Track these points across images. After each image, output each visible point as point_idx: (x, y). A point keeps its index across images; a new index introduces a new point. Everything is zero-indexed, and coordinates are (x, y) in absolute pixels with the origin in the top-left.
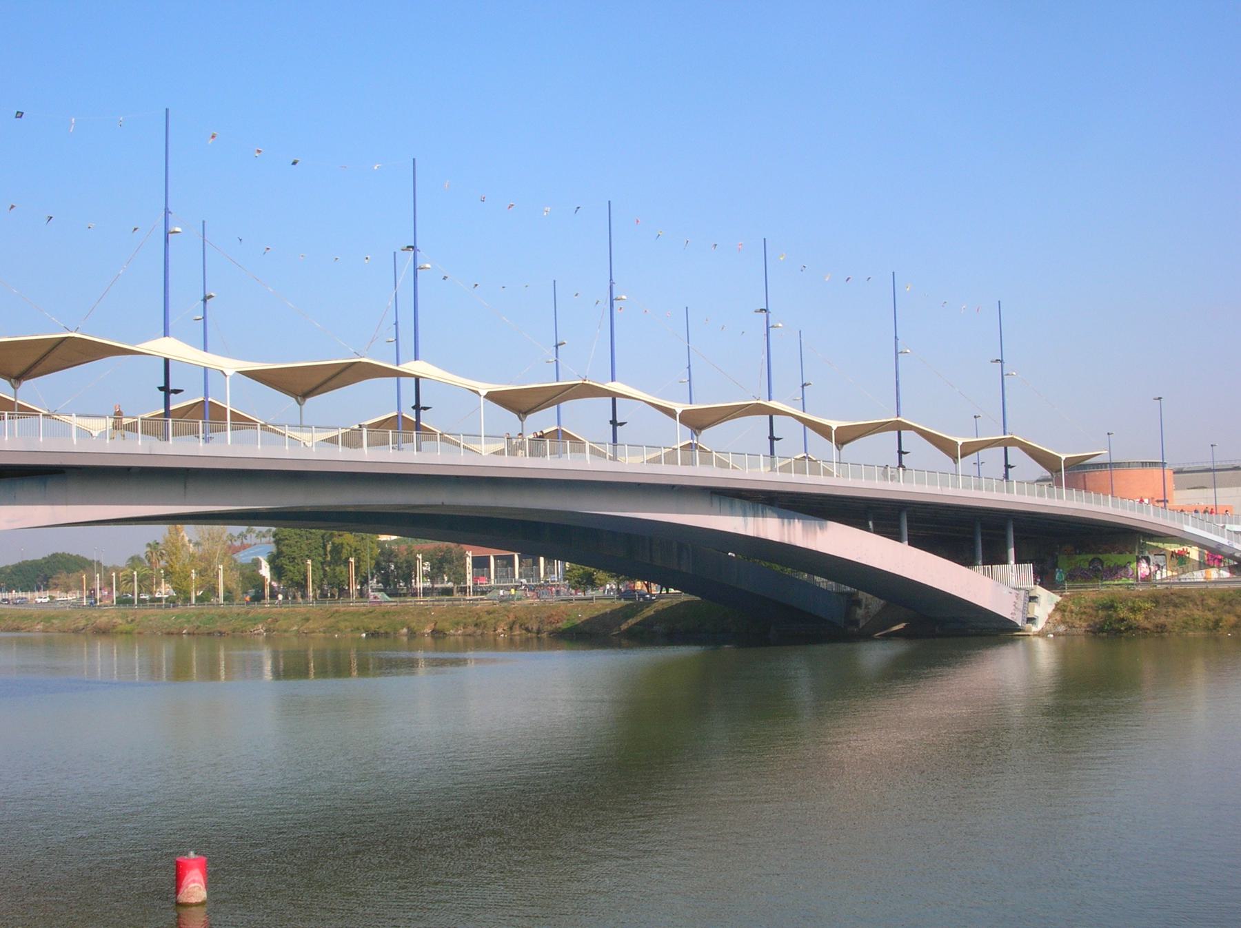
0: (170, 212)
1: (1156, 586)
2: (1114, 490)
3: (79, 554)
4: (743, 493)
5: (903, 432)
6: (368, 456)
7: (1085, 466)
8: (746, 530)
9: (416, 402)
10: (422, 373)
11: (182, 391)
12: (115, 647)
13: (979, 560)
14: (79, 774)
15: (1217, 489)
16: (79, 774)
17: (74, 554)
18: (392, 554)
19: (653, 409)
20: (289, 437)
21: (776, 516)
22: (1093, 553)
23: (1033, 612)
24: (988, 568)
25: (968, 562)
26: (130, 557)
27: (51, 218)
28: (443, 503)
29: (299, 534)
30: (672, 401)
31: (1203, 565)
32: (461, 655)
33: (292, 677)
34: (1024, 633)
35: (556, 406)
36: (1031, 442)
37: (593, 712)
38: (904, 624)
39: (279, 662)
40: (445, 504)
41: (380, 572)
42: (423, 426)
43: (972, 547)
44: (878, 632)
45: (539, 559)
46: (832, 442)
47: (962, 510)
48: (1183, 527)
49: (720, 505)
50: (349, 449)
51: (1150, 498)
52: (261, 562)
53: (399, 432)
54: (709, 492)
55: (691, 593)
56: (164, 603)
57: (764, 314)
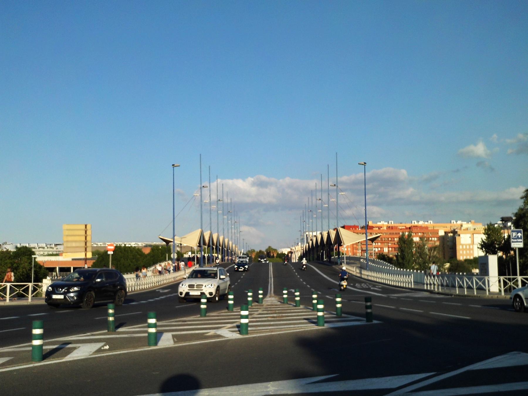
1: (227, 256)
2: (202, 170)
3: (118, 244)
4: (402, 299)
6: (349, 316)
10: (339, 231)
12: (380, 290)
13: (252, 177)
14: (232, 236)
16: (232, 236)
17: (144, 252)
19: (430, 392)
22: (100, 268)
24: (67, 233)
28: (48, 260)
29: (439, 260)
36: (165, 237)
38: (13, 358)
41: (341, 273)
42: (365, 318)
43: (199, 276)
45: (106, 330)
46: (342, 252)
48: (221, 236)
51: (388, 238)
54: (205, 187)
55: (168, 289)
57: (300, 232)
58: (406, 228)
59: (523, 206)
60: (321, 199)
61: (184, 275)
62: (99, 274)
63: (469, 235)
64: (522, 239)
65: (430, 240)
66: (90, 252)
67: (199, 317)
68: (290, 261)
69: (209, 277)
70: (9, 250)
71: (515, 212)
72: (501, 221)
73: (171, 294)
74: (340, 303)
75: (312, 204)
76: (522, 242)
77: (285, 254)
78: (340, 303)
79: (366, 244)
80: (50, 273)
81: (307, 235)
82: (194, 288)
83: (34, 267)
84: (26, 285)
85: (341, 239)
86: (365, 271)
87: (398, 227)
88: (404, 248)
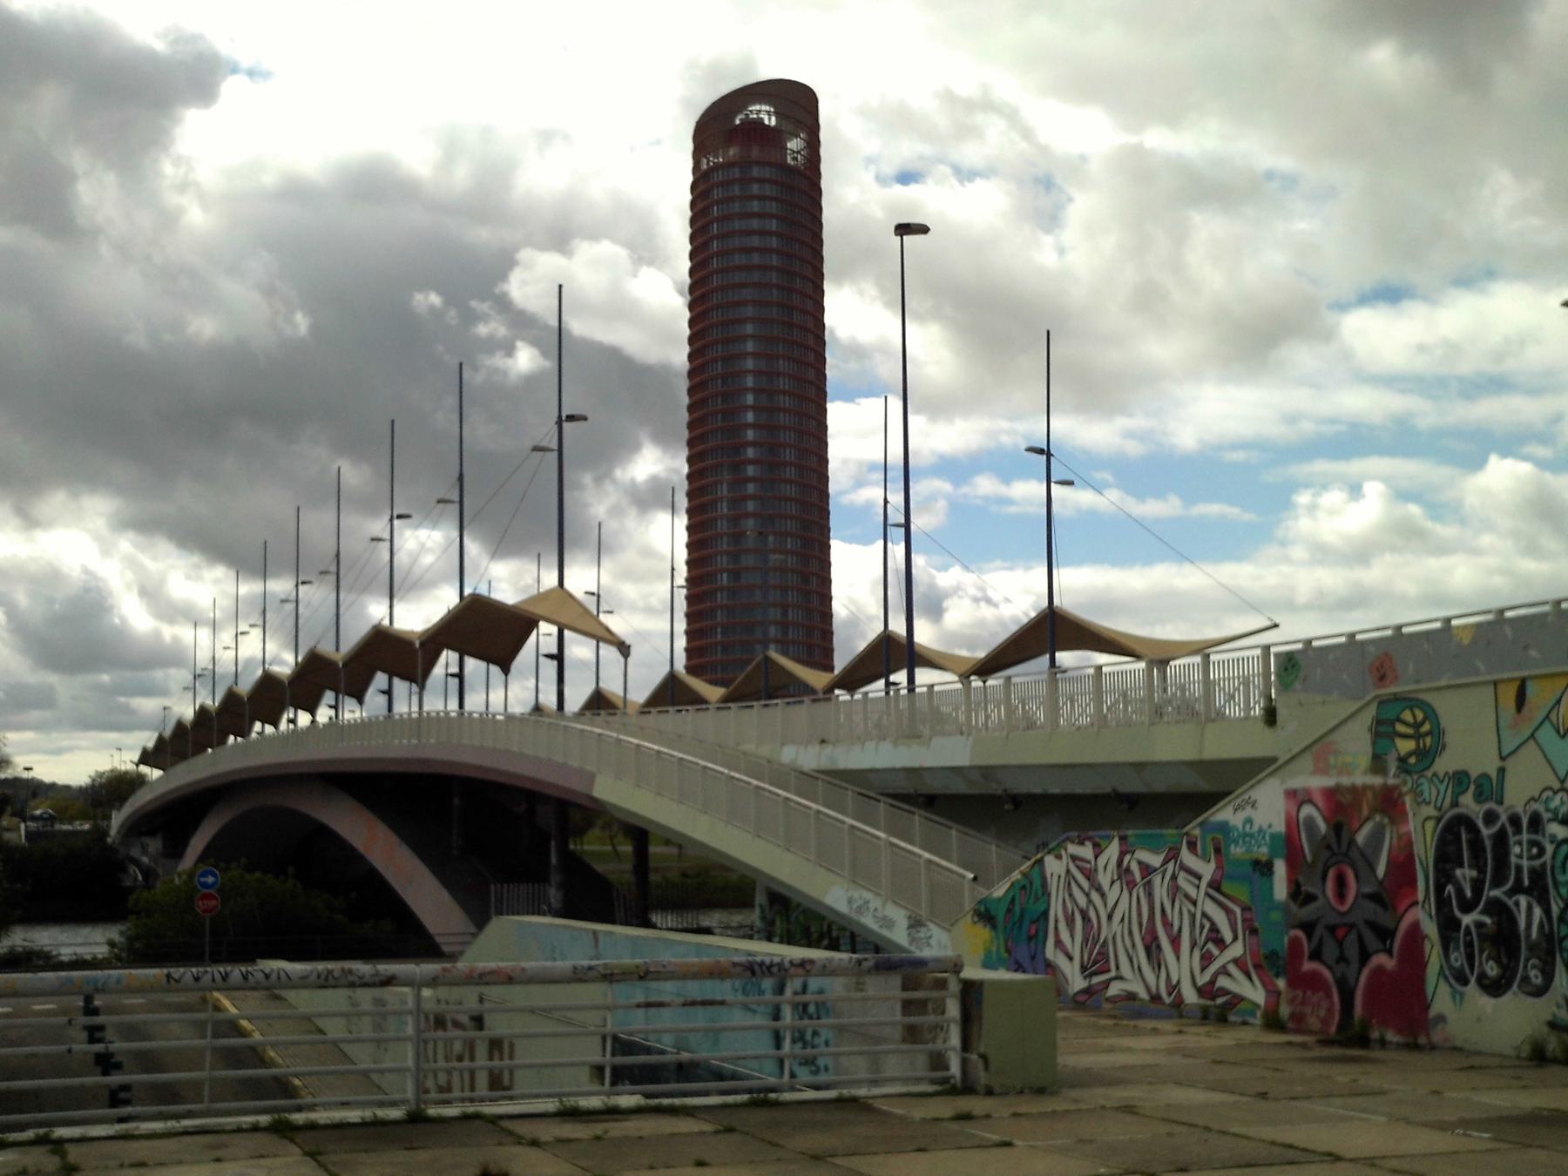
0: (1052, 455)
5: (601, 644)
7: (777, 1104)
8: (605, 612)
9: (1049, 603)
10: (941, 824)
11: (585, 419)
15: (1060, 570)
18: (1329, 847)
20: (1071, 958)
21: (915, 645)
23: (746, 453)
25: (996, 969)
26: (893, 229)
27: (1276, 626)
30: (1255, 776)
31: (175, 849)
32: (802, 699)
33: (580, 968)
34: (188, 1016)
35: (541, 590)
37: (1236, 834)
39: (667, 1097)
40: (232, 574)
44: (548, 855)
47: (626, 744)
49: (409, 572)
50: (906, 926)
52: (122, 825)
53: (865, 999)
56: (719, 637)
73: (1508, 881)
83: (632, 1040)
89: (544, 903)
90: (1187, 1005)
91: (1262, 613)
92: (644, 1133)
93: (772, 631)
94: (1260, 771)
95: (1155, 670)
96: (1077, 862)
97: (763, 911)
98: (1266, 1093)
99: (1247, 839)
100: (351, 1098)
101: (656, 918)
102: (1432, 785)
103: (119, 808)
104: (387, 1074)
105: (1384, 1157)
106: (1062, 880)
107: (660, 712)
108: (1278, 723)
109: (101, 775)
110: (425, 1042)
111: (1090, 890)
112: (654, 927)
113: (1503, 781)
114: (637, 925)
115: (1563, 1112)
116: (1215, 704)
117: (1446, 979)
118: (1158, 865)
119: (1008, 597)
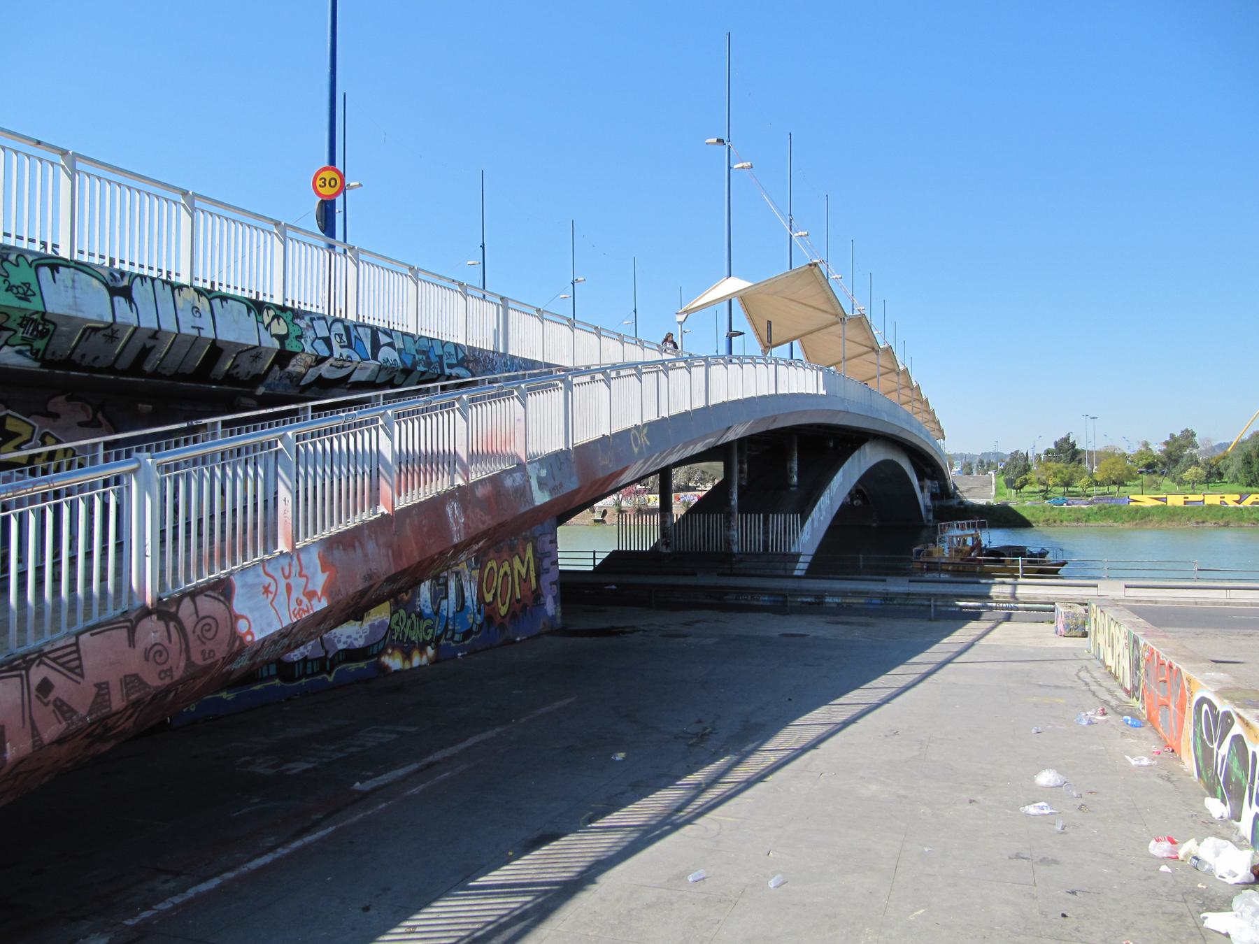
11: (744, 334)
58: (1079, 796)
59: (257, 357)
60: (726, 139)
61: (1201, 483)
62: (1165, 649)
63: (511, 352)
64: (42, 370)
65: (271, 663)
66: (163, 332)
67: (834, 594)
68: (605, 465)
69: (76, 535)
70: (1178, 434)
71: (1249, 871)
72: (355, 552)
74: (1036, 795)
75: (182, 362)
76: (292, 620)
77: (689, 411)
78: (1036, 795)
79: (708, 365)
80: (667, 513)
81: (512, 393)
82: (136, 448)
83: (469, 638)
84: (1215, 741)
85: (869, 577)
86: (535, 453)
87: (1028, 548)
88: (371, 536)
89: (970, 555)
90: (142, 328)
91: (48, 744)
92: (147, 547)
93: (69, 721)
94: (710, 287)
95: (471, 884)
96: (59, 661)
97: (1192, 658)
98: (970, 802)
99: (670, 346)
100: (269, 527)
101: (835, 605)
102: (483, 924)
103: (306, 679)
104: (229, 301)
105: (679, 809)
106: (912, 578)
107: (910, 581)
108: (43, 677)
109: (584, 890)
110: (930, 600)
111: (321, 596)
112: (1126, 486)
113: (714, 301)
114: (61, 566)
115: (1258, 432)
116: (862, 604)
117: (736, 786)
118: (491, 599)
119: (361, 188)
